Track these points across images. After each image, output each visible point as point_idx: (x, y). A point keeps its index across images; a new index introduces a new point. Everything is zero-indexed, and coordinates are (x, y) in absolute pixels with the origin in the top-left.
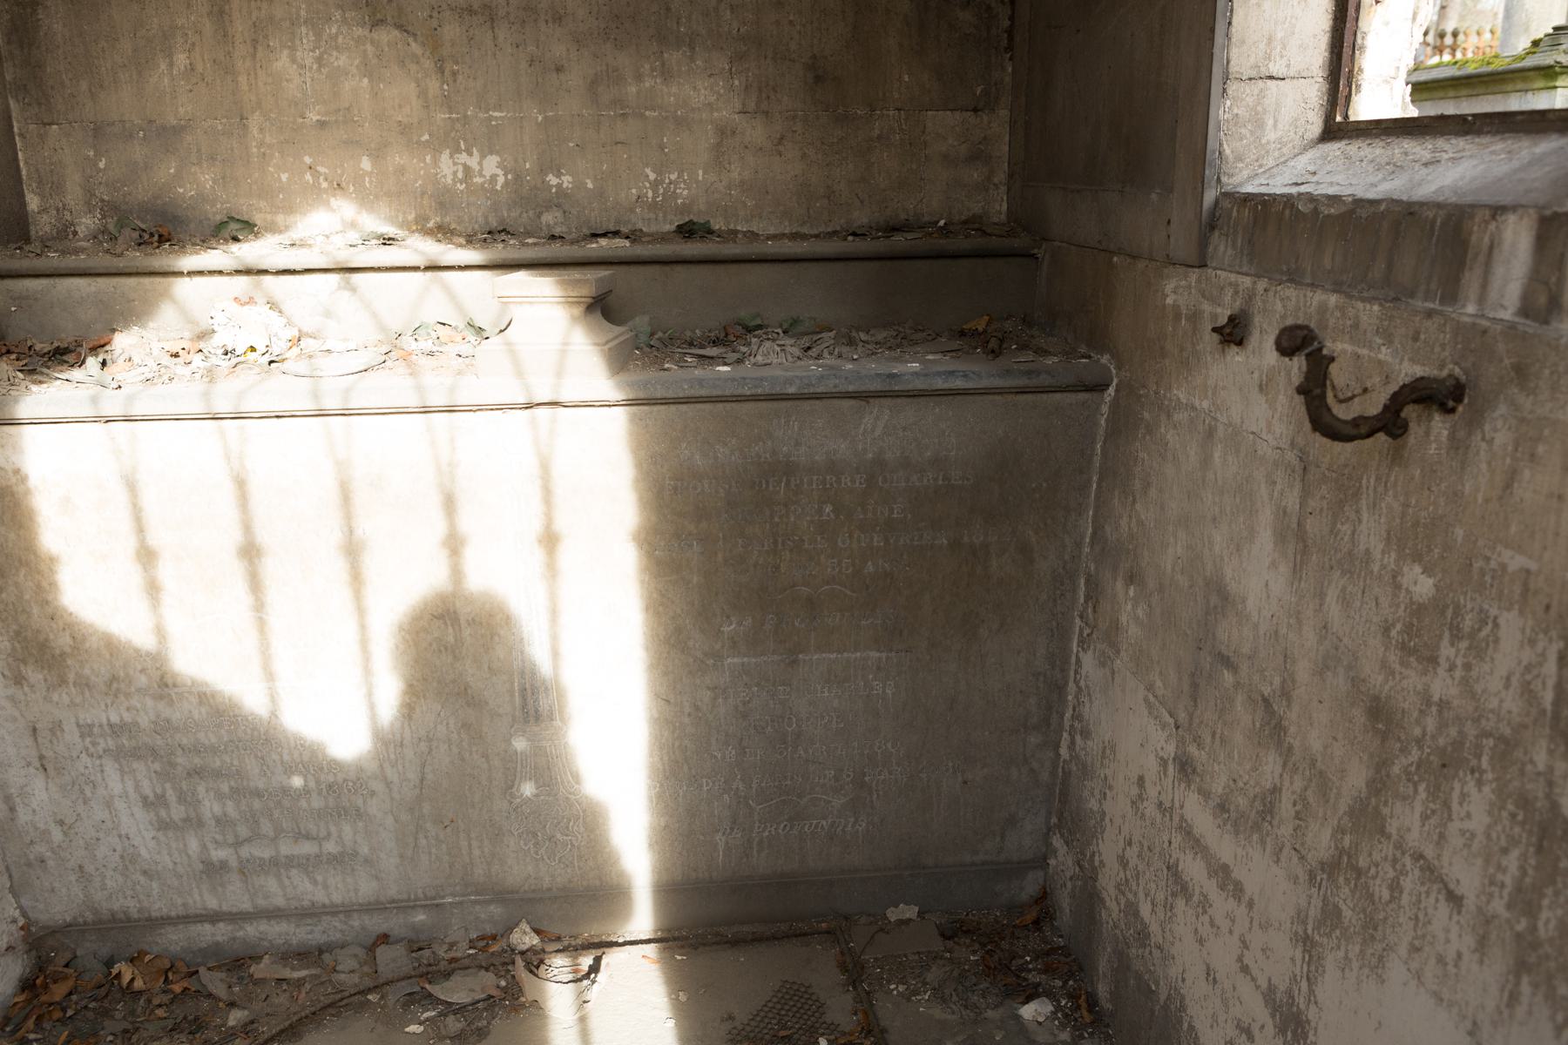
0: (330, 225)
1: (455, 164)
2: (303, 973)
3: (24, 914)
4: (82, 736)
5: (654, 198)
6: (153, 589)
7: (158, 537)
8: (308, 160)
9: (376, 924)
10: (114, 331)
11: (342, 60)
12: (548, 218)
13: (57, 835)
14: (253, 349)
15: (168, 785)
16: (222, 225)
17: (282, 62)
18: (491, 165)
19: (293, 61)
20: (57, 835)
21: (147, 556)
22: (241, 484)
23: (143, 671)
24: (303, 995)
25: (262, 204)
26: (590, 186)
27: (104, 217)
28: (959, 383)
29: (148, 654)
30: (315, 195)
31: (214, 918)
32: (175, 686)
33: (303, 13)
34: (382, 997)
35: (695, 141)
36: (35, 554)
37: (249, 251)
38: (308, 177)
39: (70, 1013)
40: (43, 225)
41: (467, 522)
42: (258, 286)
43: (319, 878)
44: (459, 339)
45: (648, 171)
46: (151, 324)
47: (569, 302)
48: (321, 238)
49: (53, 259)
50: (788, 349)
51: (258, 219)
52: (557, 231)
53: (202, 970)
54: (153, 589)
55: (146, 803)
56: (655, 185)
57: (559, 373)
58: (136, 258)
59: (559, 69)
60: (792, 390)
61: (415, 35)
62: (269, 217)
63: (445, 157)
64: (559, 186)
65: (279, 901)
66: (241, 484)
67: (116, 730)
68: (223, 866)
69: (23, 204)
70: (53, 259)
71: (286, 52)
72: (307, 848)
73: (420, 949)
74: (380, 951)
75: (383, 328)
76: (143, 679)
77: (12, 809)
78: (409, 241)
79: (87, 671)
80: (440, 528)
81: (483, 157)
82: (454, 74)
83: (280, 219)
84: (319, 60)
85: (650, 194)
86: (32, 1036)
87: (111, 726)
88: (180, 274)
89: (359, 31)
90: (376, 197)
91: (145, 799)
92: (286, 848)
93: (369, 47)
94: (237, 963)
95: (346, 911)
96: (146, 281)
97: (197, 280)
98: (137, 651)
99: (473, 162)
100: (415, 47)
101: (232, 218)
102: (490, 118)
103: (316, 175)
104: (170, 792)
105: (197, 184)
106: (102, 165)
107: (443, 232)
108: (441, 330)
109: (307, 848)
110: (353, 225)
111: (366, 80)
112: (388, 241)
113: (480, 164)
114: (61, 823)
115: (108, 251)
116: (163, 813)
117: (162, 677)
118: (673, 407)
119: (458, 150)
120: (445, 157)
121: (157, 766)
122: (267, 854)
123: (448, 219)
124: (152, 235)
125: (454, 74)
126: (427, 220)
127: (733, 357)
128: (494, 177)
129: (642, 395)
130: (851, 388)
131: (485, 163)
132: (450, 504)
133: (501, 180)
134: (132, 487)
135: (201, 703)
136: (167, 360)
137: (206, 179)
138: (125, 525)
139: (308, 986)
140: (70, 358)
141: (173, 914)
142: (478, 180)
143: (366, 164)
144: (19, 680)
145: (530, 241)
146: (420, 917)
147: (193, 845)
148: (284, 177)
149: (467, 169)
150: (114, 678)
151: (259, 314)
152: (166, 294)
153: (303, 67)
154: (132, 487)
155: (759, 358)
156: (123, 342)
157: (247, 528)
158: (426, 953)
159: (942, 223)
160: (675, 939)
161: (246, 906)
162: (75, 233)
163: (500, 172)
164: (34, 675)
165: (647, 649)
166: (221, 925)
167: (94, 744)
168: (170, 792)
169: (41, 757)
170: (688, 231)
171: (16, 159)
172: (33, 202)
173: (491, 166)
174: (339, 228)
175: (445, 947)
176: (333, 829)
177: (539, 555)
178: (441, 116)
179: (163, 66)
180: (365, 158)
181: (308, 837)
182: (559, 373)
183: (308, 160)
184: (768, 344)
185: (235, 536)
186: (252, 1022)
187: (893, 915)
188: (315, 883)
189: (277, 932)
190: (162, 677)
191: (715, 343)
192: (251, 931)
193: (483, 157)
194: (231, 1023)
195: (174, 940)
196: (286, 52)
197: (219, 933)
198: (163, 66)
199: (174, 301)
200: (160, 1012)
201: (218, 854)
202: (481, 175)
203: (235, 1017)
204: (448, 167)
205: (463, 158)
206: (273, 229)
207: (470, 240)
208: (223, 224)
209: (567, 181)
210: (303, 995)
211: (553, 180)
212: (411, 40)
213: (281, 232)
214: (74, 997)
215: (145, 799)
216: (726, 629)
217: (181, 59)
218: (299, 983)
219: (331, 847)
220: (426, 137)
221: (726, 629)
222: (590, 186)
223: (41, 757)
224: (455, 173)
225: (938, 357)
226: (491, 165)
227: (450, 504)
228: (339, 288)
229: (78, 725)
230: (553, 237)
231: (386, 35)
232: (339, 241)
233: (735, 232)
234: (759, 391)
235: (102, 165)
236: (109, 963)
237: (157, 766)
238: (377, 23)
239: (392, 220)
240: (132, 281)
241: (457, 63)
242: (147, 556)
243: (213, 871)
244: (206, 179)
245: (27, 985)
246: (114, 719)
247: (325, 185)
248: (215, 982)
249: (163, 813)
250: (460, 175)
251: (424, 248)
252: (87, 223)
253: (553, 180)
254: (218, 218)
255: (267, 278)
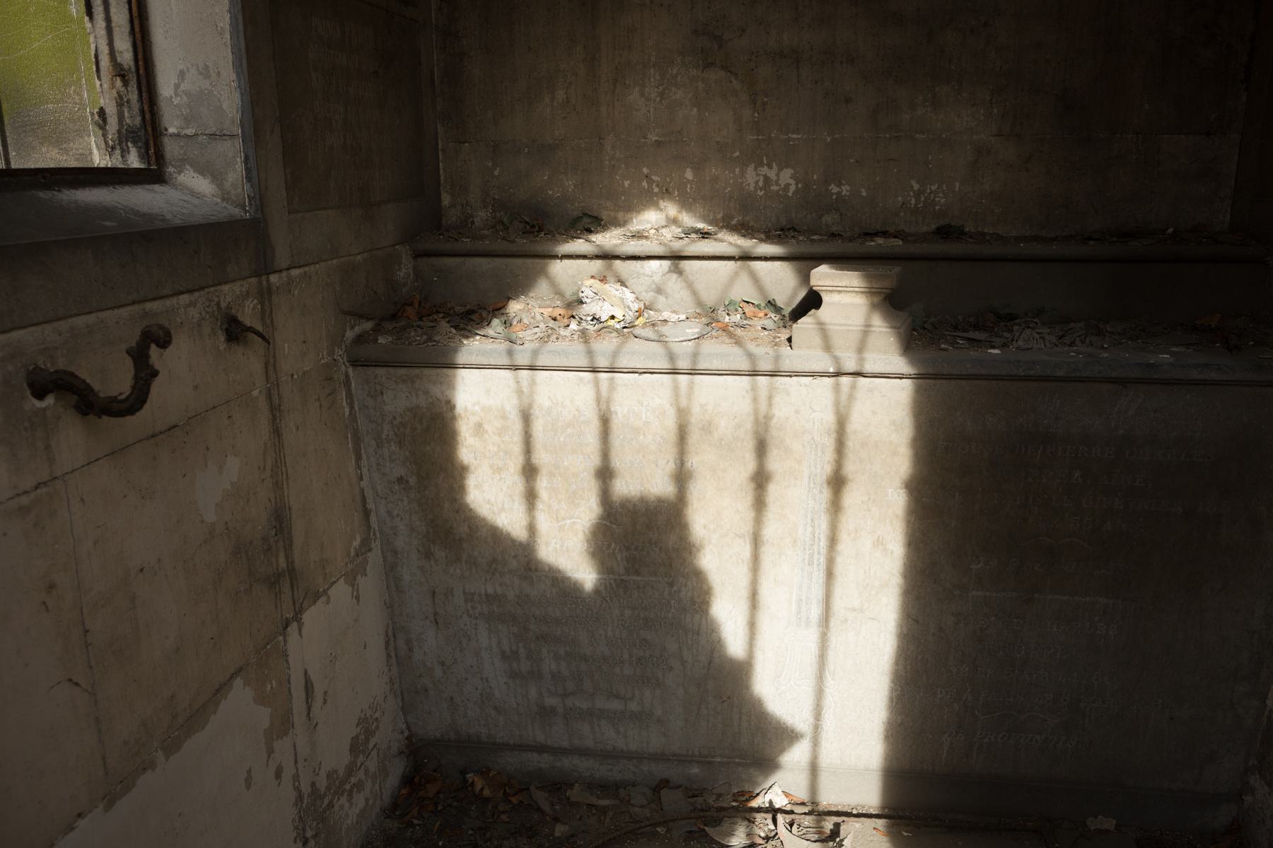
0: (657, 222)
1: (758, 175)
2: (605, 802)
3: (409, 728)
4: (466, 601)
5: (916, 204)
6: (531, 497)
7: (541, 457)
8: (645, 170)
9: (661, 771)
10: (509, 299)
11: (679, 94)
12: (827, 219)
13: (438, 672)
14: (613, 317)
15: (521, 645)
16: (578, 219)
17: (634, 96)
18: (786, 176)
19: (642, 95)
20: (438, 672)
21: (530, 471)
22: (605, 423)
23: (515, 557)
24: (608, 820)
25: (609, 204)
26: (864, 194)
27: (494, 211)
28: (1214, 375)
29: (521, 544)
30: (648, 199)
31: (541, 749)
32: (536, 570)
33: (653, 59)
34: (668, 831)
35: (957, 155)
36: (453, 465)
37: (608, 239)
38: (645, 184)
39: (440, 808)
40: (452, 216)
41: (774, 463)
42: (610, 267)
43: (621, 730)
44: (761, 315)
45: (913, 183)
46: (531, 294)
47: (870, 292)
48: (653, 231)
49: (467, 243)
50: (1047, 337)
51: (604, 215)
52: (834, 229)
53: (532, 788)
54: (531, 497)
55: (504, 656)
56: (918, 195)
57: (861, 349)
58: (522, 243)
59: (848, 101)
60: (1060, 373)
61: (736, 74)
62: (612, 214)
63: (750, 171)
64: (839, 193)
65: (590, 743)
66: (605, 423)
67: (491, 599)
68: (553, 710)
69: (439, 200)
70: (467, 243)
71: (637, 89)
72: (616, 705)
73: (694, 796)
74: (664, 792)
75: (700, 303)
76: (515, 563)
77: (411, 650)
78: (720, 236)
79: (476, 553)
80: (750, 465)
81: (780, 169)
82: (764, 104)
83: (620, 215)
84: (662, 95)
85: (913, 201)
86: (416, 822)
87: (487, 595)
88: (555, 257)
89: (694, 72)
90: (694, 200)
91: (503, 653)
92: (601, 703)
93: (700, 85)
94: (557, 785)
95: (638, 757)
96: (529, 261)
97: (567, 262)
98: (513, 541)
99: (772, 174)
100: (736, 84)
101: (585, 214)
102: (789, 139)
103: (650, 182)
104: (522, 650)
105: (564, 188)
106: (496, 173)
107: (744, 229)
108: (748, 309)
109: (616, 705)
110: (675, 221)
111: (695, 110)
112: (705, 235)
113: (777, 175)
114: (443, 664)
115: (504, 238)
116: (515, 665)
117: (528, 563)
118: (954, 382)
119: (761, 164)
120: (750, 171)
121: (515, 629)
122: (585, 705)
123: (747, 218)
124: (533, 227)
125: (764, 104)
126: (732, 218)
127: (998, 341)
128: (787, 186)
129: (931, 371)
130: (1114, 374)
131: (782, 174)
132: (761, 448)
133: (793, 188)
134: (526, 418)
135: (553, 585)
136: (551, 324)
137: (570, 184)
138: (517, 449)
139: (611, 814)
140: (474, 317)
141: (512, 742)
142: (774, 188)
143: (689, 175)
144: (428, 555)
145: (815, 237)
146: (695, 770)
147: (533, 692)
148: (627, 183)
149: (766, 178)
150: (495, 560)
151: (612, 289)
152: (543, 272)
153: (648, 99)
154: (526, 418)
155: (1021, 343)
156: (514, 307)
157: (605, 454)
158: (700, 800)
159: (1170, 230)
160: (900, 818)
161: (565, 744)
162: (473, 223)
163: (792, 182)
164: (440, 553)
165: (588, 541)
166: (545, 755)
167: (473, 608)
168: (522, 650)
169: (436, 614)
170: (945, 232)
171: (438, 169)
172: (446, 200)
173: (786, 177)
174: (664, 223)
175: (714, 797)
176: (637, 692)
177: (826, 494)
178: (750, 137)
179: (547, 100)
180: (688, 170)
181: (617, 697)
182: (861, 349)
183: (645, 170)
184: (1028, 331)
185: (595, 461)
186: (572, 836)
187: (1093, 824)
188: (618, 733)
189: (585, 766)
190: (528, 563)
191: (976, 327)
192: (567, 763)
193: (780, 169)
194: (557, 834)
195: (510, 761)
196: (637, 89)
197: (544, 761)
198: (547, 100)
199: (548, 277)
200: (504, 817)
201: (550, 701)
202: (777, 184)
203: (560, 830)
204: (751, 178)
205: (765, 170)
206: (617, 223)
207: (768, 237)
208: (579, 219)
209: (845, 189)
210: (608, 820)
211: (834, 189)
212: (733, 78)
213: (620, 226)
214: (441, 796)
215: (503, 653)
216: (974, 567)
217: (560, 94)
218: (604, 810)
219: (633, 706)
220: (737, 154)
221: (974, 567)
222: (864, 194)
223: (436, 614)
224: (757, 182)
225: (1182, 349)
226: (786, 176)
227: (761, 448)
228: (670, 271)
229: (464, 593)
230: (833, 235)
231: (715, 75)
232: (668, 234)
233: (983, 234)
234: (1032, 373)
235: (496, 173)
236: (464, 772)
237: (515, 629)
238: (708, 65)
239: (704, 218)
240: (519, 261)
241: (767, 96)
242: (530, 471)
243: (545, 713)
244: (570, 184)
245: (408, 781)
246: (490, 591)
247: (656, 190)
248: (541, 798)
249: (515, 665)
250: (761, 184)
251: (730, 242)
252: (482, 216)
253: (834, 189)
254: (576, 213)
255: (618, 263)
